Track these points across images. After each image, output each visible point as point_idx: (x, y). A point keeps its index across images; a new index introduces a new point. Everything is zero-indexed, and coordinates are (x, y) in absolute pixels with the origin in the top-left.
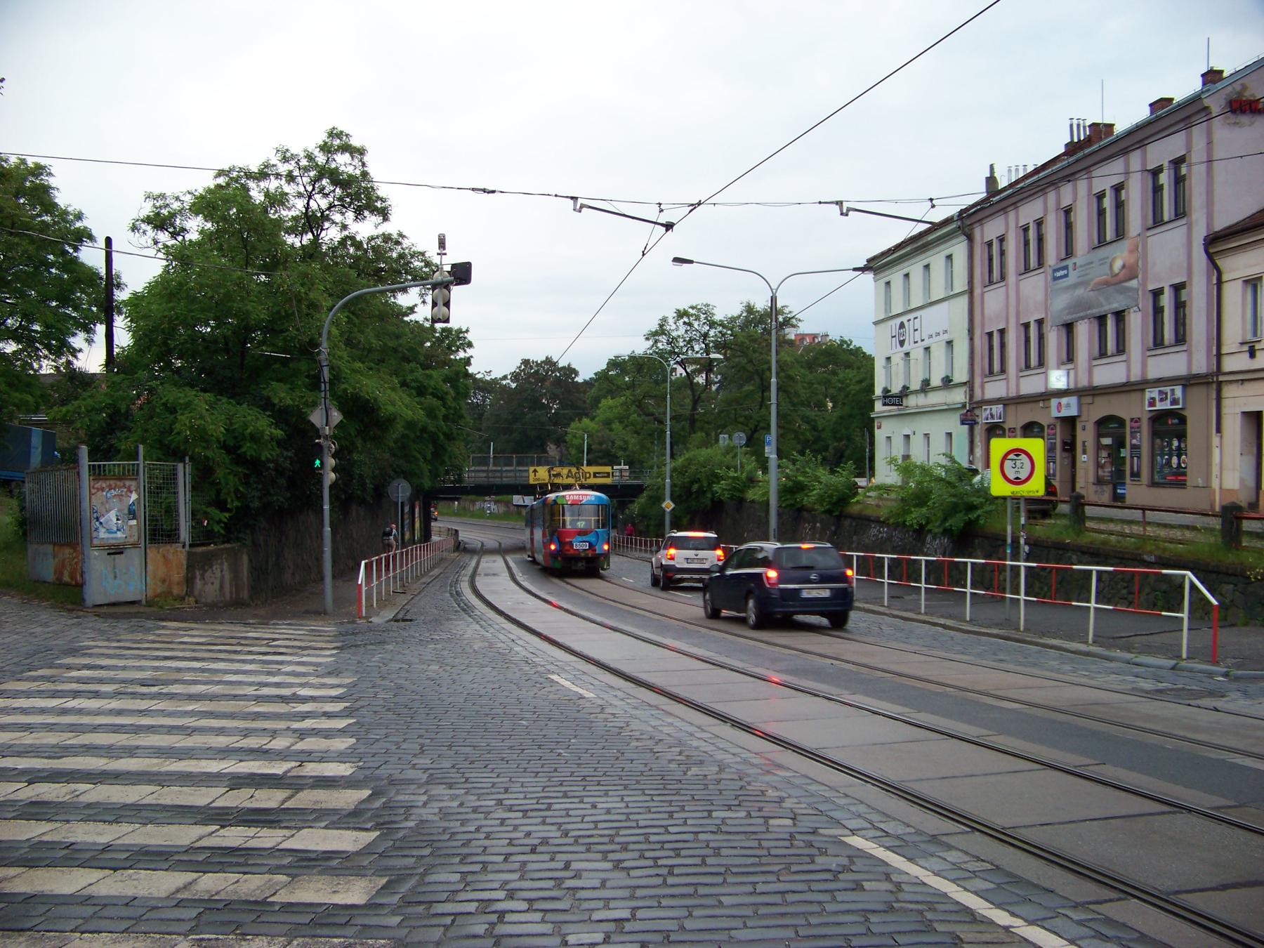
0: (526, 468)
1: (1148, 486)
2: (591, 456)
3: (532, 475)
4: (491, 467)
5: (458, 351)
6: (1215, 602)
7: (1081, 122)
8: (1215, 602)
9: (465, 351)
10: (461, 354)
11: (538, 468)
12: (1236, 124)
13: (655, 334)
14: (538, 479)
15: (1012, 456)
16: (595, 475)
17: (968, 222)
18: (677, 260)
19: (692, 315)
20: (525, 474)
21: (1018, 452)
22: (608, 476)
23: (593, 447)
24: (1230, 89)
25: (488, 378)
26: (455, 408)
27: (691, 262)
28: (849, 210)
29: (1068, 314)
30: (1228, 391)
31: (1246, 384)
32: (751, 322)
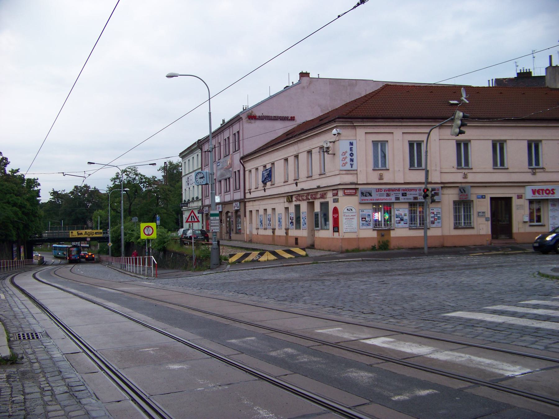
0: (68, 231)
1: (235, 234)
2: (102, 225)
3: (71, 234)
4: (62, 231)
5: (34, 187)
6: (156, 263)
7: (247, 107)
8: (156, 263)
9: (37, 187)
10: (36, 189)
11: (73, 231)
12: (250, 122)
13: (115, 179)
14: (73, 236)
15: (147, 228)
16: (96, 233)
17: (201, 144)
18: (89, 163)
19: (128, 171)
20: (68, 234)
21: (148, 227)
22: (101, 234)
23: (103, 221)
24: (248, 112)
25: (64, 193)
26: (33, 209)
27: (94, 163)
28: (65, 174)
29: (221, 178)
30: (247, 204)
31: (250, 202)
32: (171, 169)
